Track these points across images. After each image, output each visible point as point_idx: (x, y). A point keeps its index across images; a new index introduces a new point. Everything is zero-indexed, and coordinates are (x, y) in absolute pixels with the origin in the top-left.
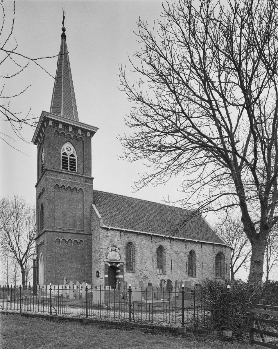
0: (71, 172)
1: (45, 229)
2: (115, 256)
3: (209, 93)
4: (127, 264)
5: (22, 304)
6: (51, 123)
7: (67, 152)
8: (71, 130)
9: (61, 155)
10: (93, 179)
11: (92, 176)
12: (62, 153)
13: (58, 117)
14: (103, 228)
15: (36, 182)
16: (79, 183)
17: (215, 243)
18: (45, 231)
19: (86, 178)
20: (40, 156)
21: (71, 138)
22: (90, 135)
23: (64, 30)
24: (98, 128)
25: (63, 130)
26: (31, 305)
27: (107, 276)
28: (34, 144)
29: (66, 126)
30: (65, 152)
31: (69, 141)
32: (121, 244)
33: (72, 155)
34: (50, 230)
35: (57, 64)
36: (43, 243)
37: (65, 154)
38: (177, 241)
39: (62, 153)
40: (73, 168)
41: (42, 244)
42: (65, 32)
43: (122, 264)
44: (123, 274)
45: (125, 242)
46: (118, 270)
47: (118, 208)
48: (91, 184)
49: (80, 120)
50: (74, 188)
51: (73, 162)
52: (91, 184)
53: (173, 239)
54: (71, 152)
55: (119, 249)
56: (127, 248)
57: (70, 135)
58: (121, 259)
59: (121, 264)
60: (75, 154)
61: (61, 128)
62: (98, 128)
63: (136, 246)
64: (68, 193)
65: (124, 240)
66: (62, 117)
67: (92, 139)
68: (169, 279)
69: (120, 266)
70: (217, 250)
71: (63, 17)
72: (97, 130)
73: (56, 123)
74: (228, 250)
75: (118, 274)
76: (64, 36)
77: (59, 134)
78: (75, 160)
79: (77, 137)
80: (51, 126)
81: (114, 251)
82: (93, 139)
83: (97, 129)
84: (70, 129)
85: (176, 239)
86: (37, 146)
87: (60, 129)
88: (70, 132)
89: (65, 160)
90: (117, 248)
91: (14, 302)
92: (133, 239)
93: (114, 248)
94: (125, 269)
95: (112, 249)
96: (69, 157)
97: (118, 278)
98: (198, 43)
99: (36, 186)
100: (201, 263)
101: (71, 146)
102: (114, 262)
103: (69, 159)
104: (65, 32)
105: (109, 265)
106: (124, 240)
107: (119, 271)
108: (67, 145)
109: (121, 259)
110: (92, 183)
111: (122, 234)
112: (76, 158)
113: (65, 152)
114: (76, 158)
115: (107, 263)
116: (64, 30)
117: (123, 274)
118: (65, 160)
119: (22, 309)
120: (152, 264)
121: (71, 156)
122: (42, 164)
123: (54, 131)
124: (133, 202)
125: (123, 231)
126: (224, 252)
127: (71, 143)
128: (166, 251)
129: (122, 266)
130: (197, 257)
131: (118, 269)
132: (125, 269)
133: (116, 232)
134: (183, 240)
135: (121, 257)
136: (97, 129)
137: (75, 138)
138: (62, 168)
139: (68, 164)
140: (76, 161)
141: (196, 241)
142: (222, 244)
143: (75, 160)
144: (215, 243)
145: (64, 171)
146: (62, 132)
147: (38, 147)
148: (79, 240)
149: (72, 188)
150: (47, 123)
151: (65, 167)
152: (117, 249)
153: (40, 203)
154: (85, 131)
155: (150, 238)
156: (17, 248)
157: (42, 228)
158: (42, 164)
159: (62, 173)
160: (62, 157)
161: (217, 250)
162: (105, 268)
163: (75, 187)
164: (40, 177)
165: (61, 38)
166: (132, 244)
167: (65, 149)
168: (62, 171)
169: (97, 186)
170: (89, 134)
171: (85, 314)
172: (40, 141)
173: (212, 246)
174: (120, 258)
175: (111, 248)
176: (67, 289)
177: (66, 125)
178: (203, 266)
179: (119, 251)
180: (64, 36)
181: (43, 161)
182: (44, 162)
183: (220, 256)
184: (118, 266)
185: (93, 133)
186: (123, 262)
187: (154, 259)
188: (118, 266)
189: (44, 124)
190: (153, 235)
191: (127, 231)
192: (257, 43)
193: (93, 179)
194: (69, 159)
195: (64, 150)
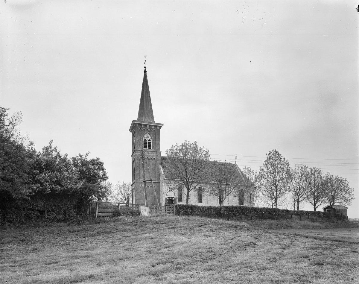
1: (135, 181)
2: (171, 194)
4: (179, 198)
6: (137, 125)
9: (143, 141)
12: (143, 140)
15: (131, 153)
18: (135, 182)
21: (148, 131)
23: (145, 68)
24: (163, 124)
25: (144, 128)
29: (151, 126)
33: (149, 140)
34: (137, 181)
37: (145, 140)
39: (143, 140)
40: (150, 147)
51: (150, 144)
62: (163, 124)
66: (144, 121)
73: (141, 125)
76: (145, 71)
78: (151, 142)
80: (137, 127)
81: (171, 191)
82: (161, 130)
87: (142, 128)
89: (145, 143)
93: (171, 189)
95: (169, 190)
96: (147, 141)
99: (132, 156)
101: (149, 135)
105: (168, 199)
108: (146, 136)
112: (151, 142)
114: (151, 142)
116: (145, 68)
121: (148, 141)
138: (144, 148)
139: (148, 145)
143: (151, 142)
151: (145, 147)
153: (133, 167)
154: (157, 126)
156: (295, 204)
160: (144, 142)
162: (166, 200)
164: (133, 151)
165: (131, 134)
170: (158, 128)
175: (169, 190)
180: (145, 71)
185: (160, 127)
186: (177, 197)
188: (173, 199)
192: (63, 242)
195: (144, 138)
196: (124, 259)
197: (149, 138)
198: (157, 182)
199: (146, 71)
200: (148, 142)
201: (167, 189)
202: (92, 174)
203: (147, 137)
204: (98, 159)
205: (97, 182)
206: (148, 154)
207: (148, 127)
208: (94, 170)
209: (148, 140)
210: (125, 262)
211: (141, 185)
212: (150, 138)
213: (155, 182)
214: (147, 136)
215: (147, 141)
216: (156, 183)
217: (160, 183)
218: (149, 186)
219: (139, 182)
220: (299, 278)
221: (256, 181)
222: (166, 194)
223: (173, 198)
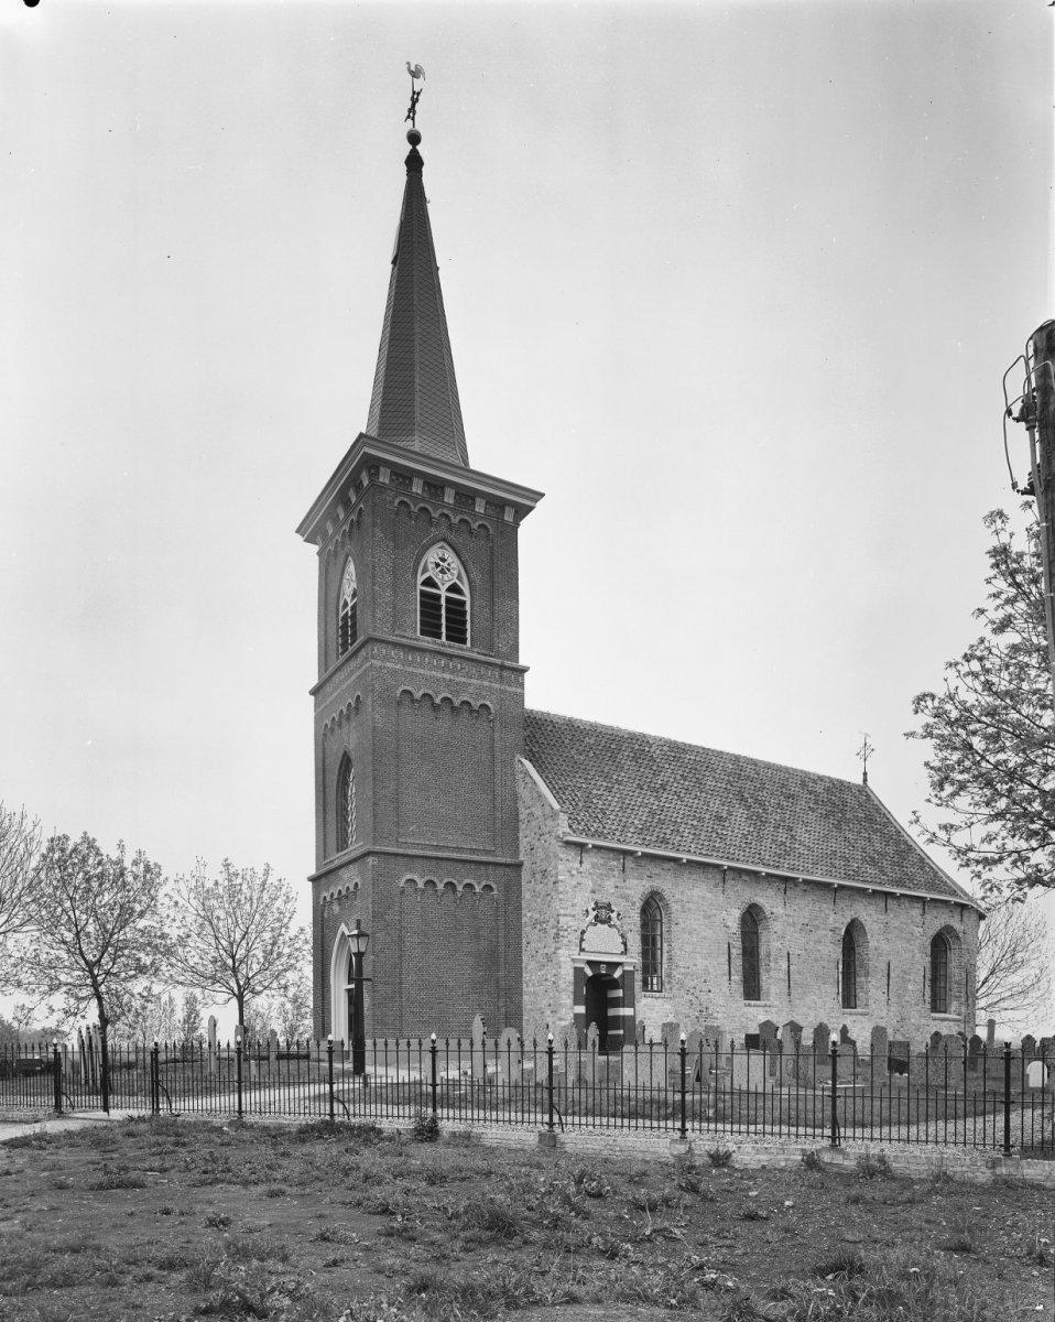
0: (450, 647)
2: (606, 944)
5: (243, 1095)
8: (451, 502)
9: (419, 587)
10: (524, 670)
11: (523, 661)
13: (420, 458)
14: (568, 843)
15: (314, 681)
16: (476, 687)
17: (929, 896)
19: (502, 667)
20: (333, 588)
21: (450, 527)
23: (414, 138)
24: (542, 495)
25: (423, 500)
26: (272, 1092)
27: (581, 1009)
28: (306, 540)
30: (430, 578)
31: (444, 540)
32: (626, 898)
33: (454, 588)
35: (394, 262)
37: (429, 582)
38: (805, 887)
39: (421, 579)
40: (457, 634)
41: (347, 897)
42: (418, 147)
43: (631, 968)
44: (632, 1005)
45: (641, 890)
46: (617, 987)
47: (606, 770)
49: (473, 465)
50: (463, 702)
51: (456, 609)
53: (794, 880)
55: (619, 915)
56: (644, 911)
57: (447, 516)
58: (626, 950)
59: (627, 968)
60: (463, 583)
61: (420, 492)
62: (542, 495)
63: (674, 907)
64: (444, 723)
65: (637, 888)
67: (520, 531)
68: (821, 1024)
69: (622, 976)
70: (938, 920)
71: (411, 94)
72: (537, 501)
74: (970, 918)
75: (617, 1003)
76: (414, 163)
77: (470, 532)
78: (463, 603)
79: (450, 520)
80: (383, 487)
81: (603, 922)
82: (527, 530)
84: (449, 498)
85: (806, 882)
86: (316, 548)
87: (415, 498)
88: (447, 506)
89: (430, 603)
90: (613, 911)
91: (257, 1086)
92: (667, 884)
93: (603, 913)
94: (638, 985)
95: (596, 917)
96: (443, 593)
97: (617, 1018)
100: (885, 966)
102: (604, 963)
104: (418, 147)
106: (836, 918)
107: (620, 993)
108: (432, 556)
109: (626, 950)
110: (522, 685)
111: (630, 864)
112: (467, 598)
113: (430, 578)
114: (467, 598)
115: (582, 965)
116: (414, 138)
117: (632, 1005)
118: (430, 603)
119: (243, 1109)
120: (727, 967)
123: (396, 504)
124: (647, 749)
125: (632, 853)
126: (958, 926)
127: (450, 545)
128: (771, 922)
129: (632, 973)
130: (873, 944)
131: (615, 984)
132: (638, 985)
133: (611, 855)
134: (827, 886)
135: (625, 944)
136: (536, 497)
137: (463, 527)
140: (468, 608)
141: (763, 870)
142: (953, 899)
143: (463, 603)
144: (932, 896)
145: (427, 642)
146: (422, 505)
147: (319, 554)
148: (479, 883)
149: (457, 703)
150: (370, 476)
151: (430, 628)
152: (614, 915)
153: (334, 763)
154: (498, 505)
155: (830, 896)
157: (342, 843)
159: (422, 650)
160: (423, 594)
161: (938, 920)
162: (576, 983)
166: (662, 899)
168: (419, 644)
169: (540, 696)
170: (509, 517)
171: (237, 1108)
173: (919, 905)
174: (623, 946)
176: (462, 1048)
177: (403, 472)
178: (892, 975)
179: (618, 923)
180: (414, 163)
181: (346, 604)
183: (941, 944)
184: (617, 974)
185: (523, 511)
186: (633, 960)
187: (733, 951)
188: (617, 974)
189: (359, 477)
190: (729, 867)
191: (645, 855)
193: (524, 670)
195: (425, 570)
196: (87, 1141)
197: (455, 572)
198: (503, 860)
199: (421, 163)
201: (578, 911)
203: (443, 567)
206: (447, 676)
207: (449, 498)
209: (447, 585)
211: (408, 877)
212: (459, 578)
213: (491, 859)
214: (443, 560)
215: (443, 593)
216: (500, 871)
217: (519, 866)
218: (440, 886)
219: (397, 855)
220: (722, 1230)
222: (575, 938)
223: (617, 965)
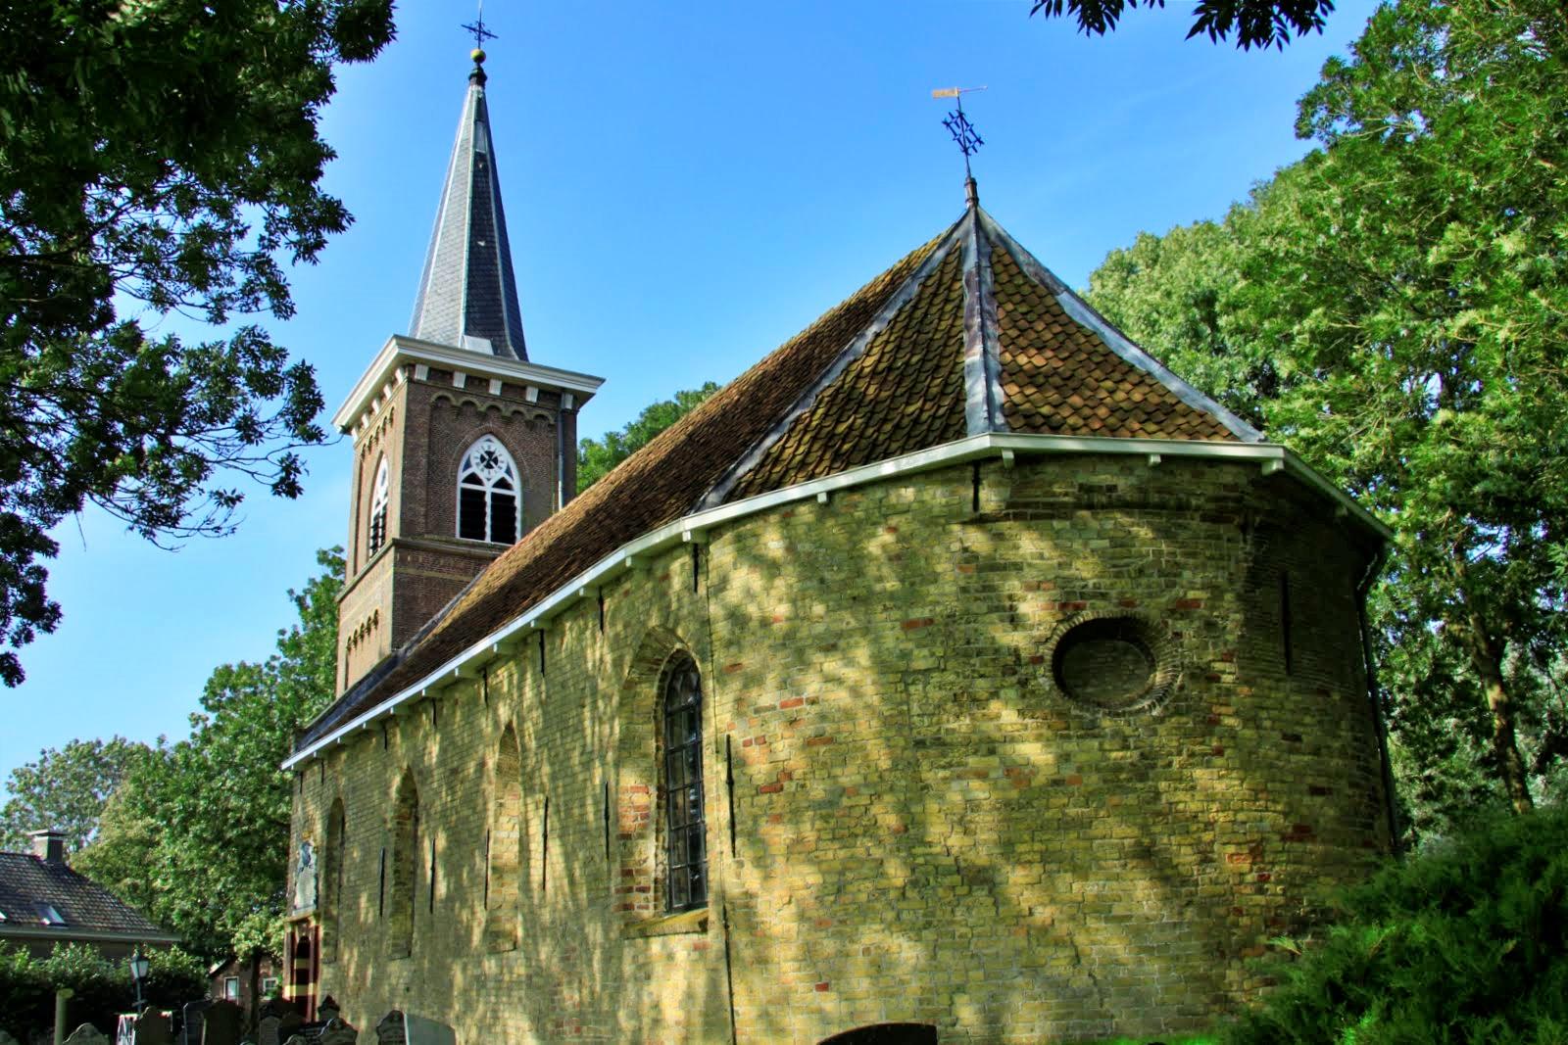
3: (429, 865)
7: (482, 475)
9: (461, 485)
12: (462, 475)
22: (574, 405)
24: (602, 381)
33: (502, 483)
36: (376, 622)
37: (473, 479)
39: (462, 475)
48: (402, 570)
52: (402, 570)
54: (497, 474)
57: (471, 404)
62: (602, 381)
67: (580, 417)
83: (331, 155)
87: (458, 392)
88: (494, 398)
96: (488, 489)
98: (873, 413)
101: (497, 447)
103: (488, 499)
108: (476, 451)
112: (516, 492)
118: (473, 501)
122: (374, 514)
123: (433, 399)
138: (462, 535)
143: (513, 498)
151: (472, 527)
154: (552, 395)
158: (374, 514)
163: (474, 400)
167: (474, 462)
172: (370, 428)
182: (385, 508)
185: (581, 398)
194: (488, 499)
195: (468, 465)
200: (494, 495)
202: (457, 905)
204: (339, 202)
205: (461, 922)
208: (273, 175)
209: (493, 481)
210: (147, 11)
212: (508, 471)
221: (810, 919)
